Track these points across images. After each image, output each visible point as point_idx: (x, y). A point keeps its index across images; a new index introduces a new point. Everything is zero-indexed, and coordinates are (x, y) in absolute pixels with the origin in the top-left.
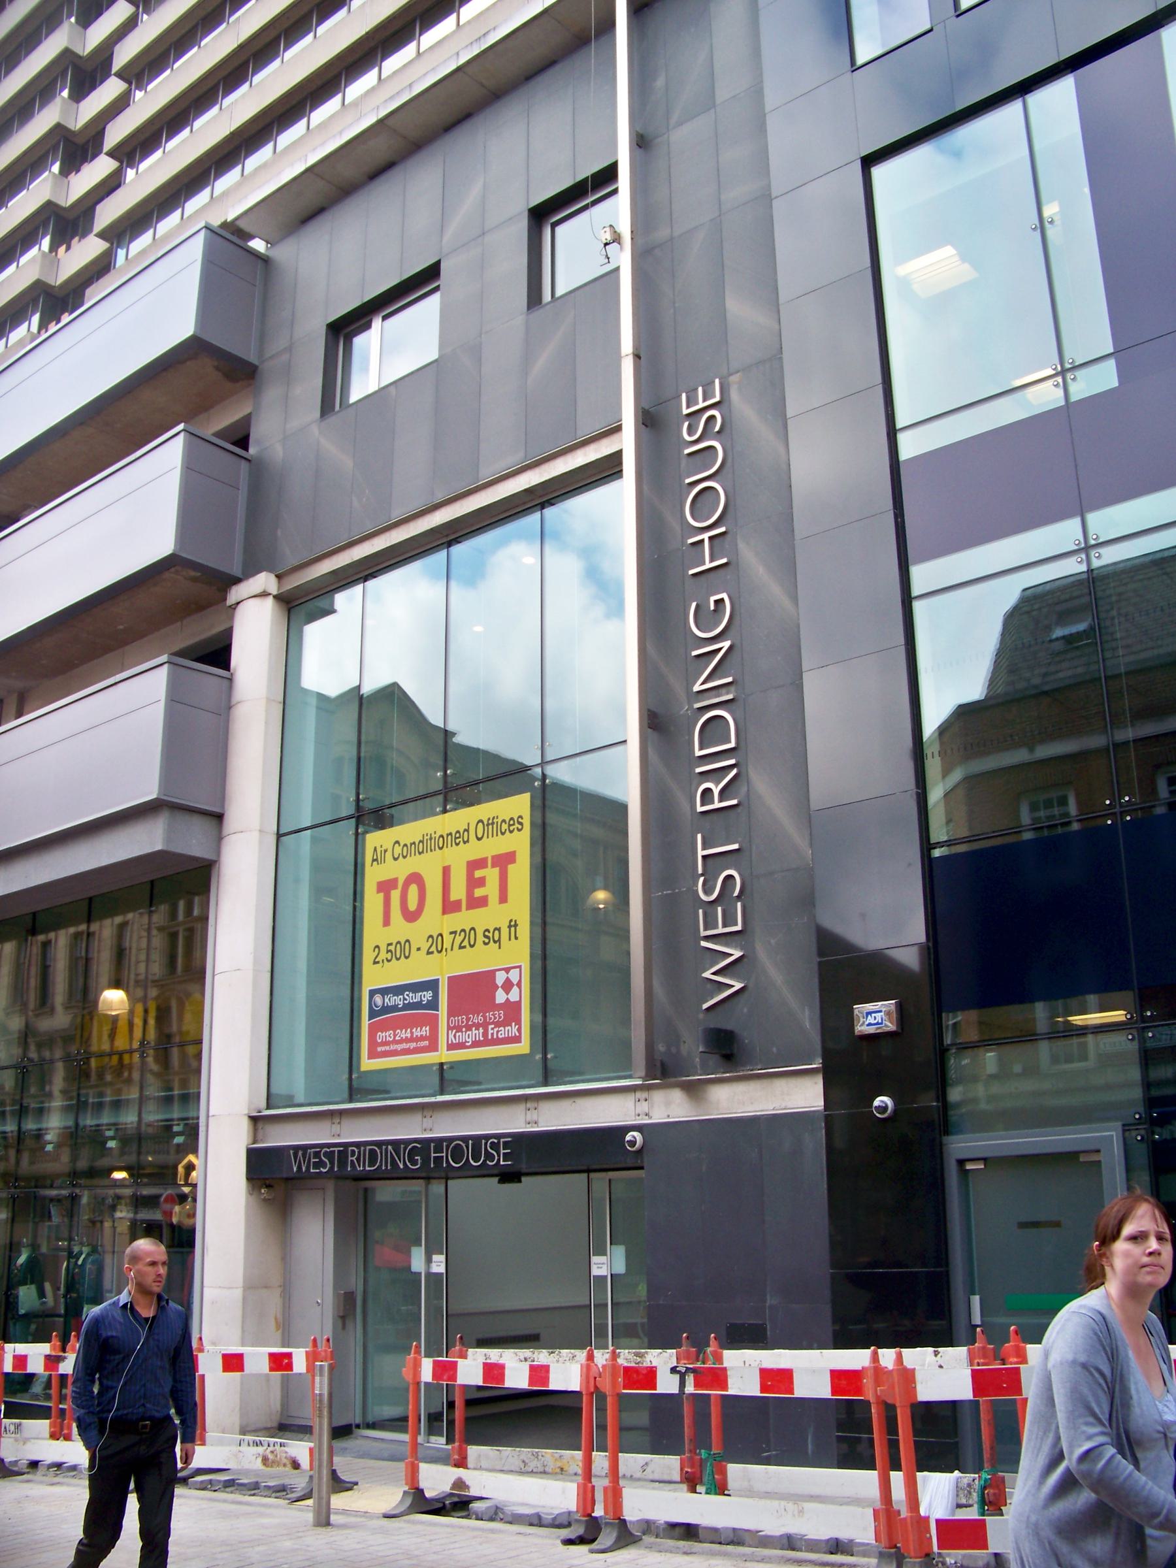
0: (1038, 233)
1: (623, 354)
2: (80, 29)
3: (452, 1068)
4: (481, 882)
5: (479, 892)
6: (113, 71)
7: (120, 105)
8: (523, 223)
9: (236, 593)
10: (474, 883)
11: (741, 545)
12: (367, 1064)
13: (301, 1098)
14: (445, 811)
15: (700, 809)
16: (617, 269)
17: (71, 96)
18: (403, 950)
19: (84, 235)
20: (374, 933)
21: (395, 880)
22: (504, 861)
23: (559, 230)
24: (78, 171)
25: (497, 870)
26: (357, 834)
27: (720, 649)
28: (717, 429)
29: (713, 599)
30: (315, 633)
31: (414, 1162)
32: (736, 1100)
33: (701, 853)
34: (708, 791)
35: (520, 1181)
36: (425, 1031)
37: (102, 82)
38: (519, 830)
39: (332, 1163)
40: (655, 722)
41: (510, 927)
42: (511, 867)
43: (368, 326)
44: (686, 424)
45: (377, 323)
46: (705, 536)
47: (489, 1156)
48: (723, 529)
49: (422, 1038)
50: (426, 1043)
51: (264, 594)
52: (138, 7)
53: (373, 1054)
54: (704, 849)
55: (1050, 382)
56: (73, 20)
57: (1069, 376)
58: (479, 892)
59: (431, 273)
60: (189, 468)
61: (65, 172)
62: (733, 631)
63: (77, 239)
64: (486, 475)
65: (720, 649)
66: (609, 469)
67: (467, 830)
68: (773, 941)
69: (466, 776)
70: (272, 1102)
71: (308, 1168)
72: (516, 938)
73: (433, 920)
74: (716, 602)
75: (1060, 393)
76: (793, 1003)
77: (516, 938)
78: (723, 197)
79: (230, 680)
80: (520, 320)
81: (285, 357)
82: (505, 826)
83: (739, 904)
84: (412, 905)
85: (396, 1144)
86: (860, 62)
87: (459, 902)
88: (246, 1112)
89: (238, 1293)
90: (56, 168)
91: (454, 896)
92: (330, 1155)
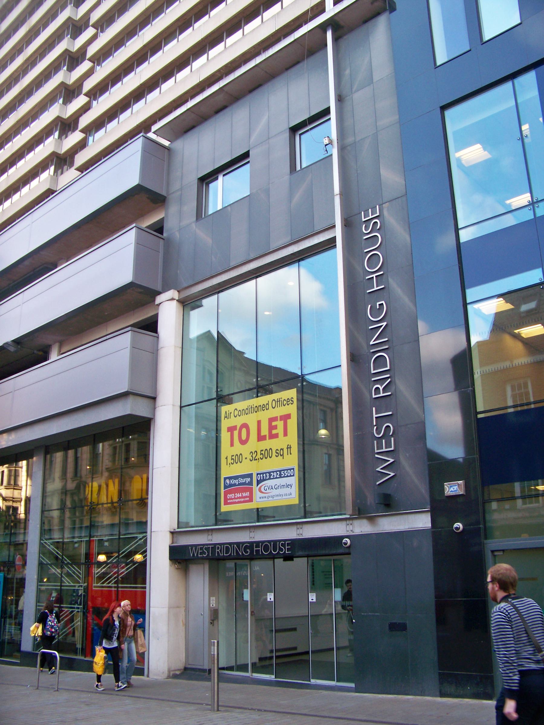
0: (520, 142)
1: (335, 194)
2: (72, 40)
3: (262, 510)
4: (276, 427)
5: (274, 432)
6: (87, 58)
7: (89, 73)
8: (287, 135)
9: (159, 299)
10: (271, 428)
11: (390, 280)
12: (224, 508)
13: (192, 523)
14: (257, 397)
15: (374, 396)
16: (332, 155)
17: (68, 70)
18: (239, 459)
19: (74, 131)
20: (226, 451)
21: (236, 427)
22: (286, 418)
23: (302, 137)
24: (71, 102)
25: (282, 422)
26: (217, 406)
27: (382, 326)
28: (378, 228)
29: (378, 303)
30: (194, 314)
31: (247, 552)
32: (390, 524)
33: (375, 416)
34: (378, 388)
35: (293, 560)
36: (247, 494)
37: (81, 63)
38: (292, 404)
39: (208, 553)
40: (354, 358)
41: (287, 448)
42: (288, 421)
43: (217, 179)
44: (364, 225)
45: (221, 178)
46: (374, 276)
47: (281, 549)
48: (382, 273)
49: (246, 497)
50: (248, 499)
51: (173, 299)
52: (98, 30)
53: (226, 503)
54: (376, 414)
55: (527, 209)
56: (69, 36)
57: (536, 205)
58: (274, 432)
59: (246, 155)
60: (138, 243)
61: (65, 103)
62: (387, 318)
63: (70, 132)
64: (273, 247)
65: (382, 326)
66: (331, 244)
67: (268, 404)
68: (407, 455)
69: (267, 380)
70: (180, 525)
71: (197, 554)
72: (291, 454)
73: (253, 444)
74: (379, 305)
75: (532, 212)
76: (416, 480)
77: (291, 454)
78: (378, 124)
79: (158, 337)
80: (287, 177)
81: (179, 193)
82: (285, 402)
83: (392, 439)
84: (244, 437)
85: (238, 544)
86: (438, 64)
87: (265, 436)
88: (169, 530)
89: (166, 610)
90: (61, 101)
91: (263, 434)
92: (207, 549)
